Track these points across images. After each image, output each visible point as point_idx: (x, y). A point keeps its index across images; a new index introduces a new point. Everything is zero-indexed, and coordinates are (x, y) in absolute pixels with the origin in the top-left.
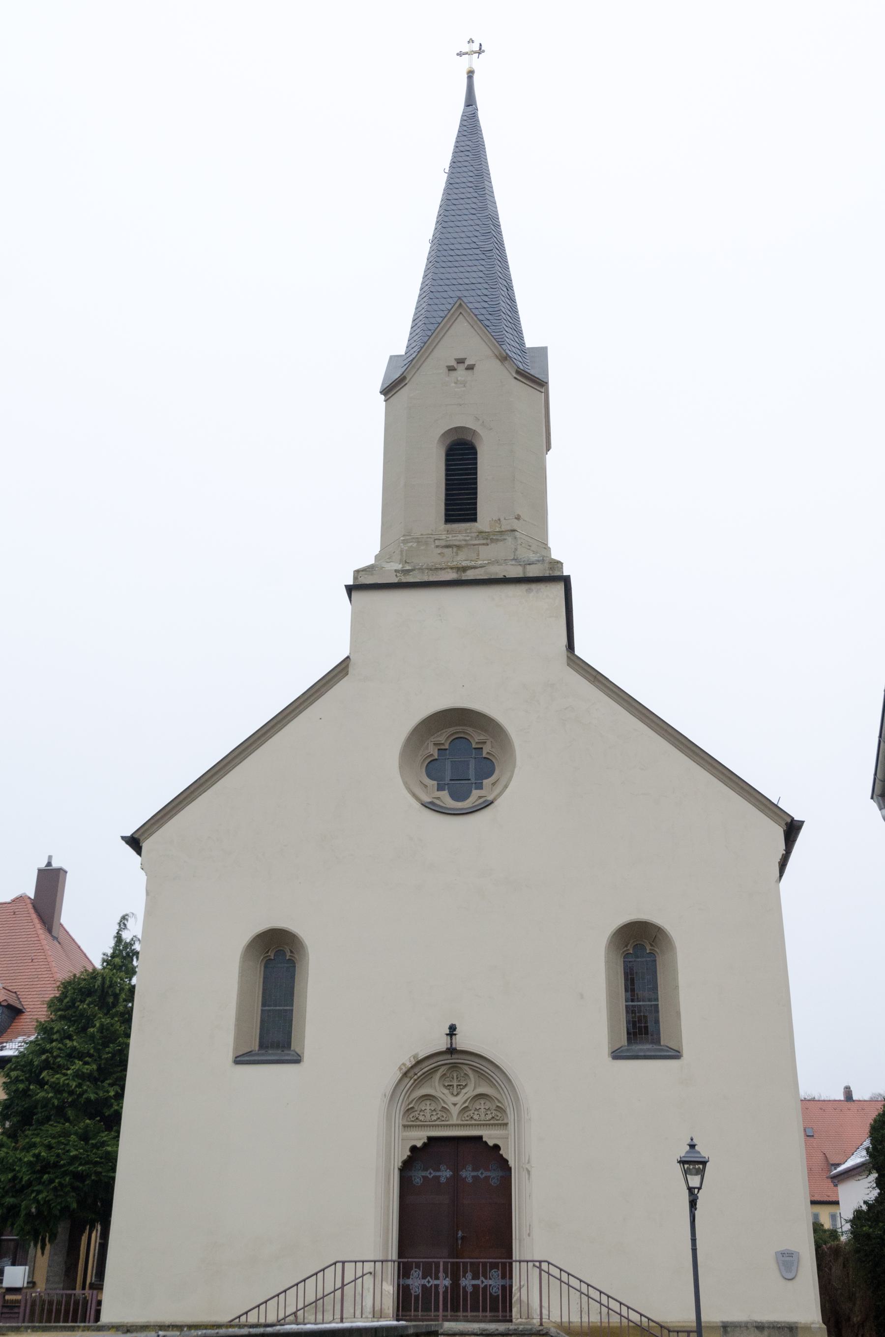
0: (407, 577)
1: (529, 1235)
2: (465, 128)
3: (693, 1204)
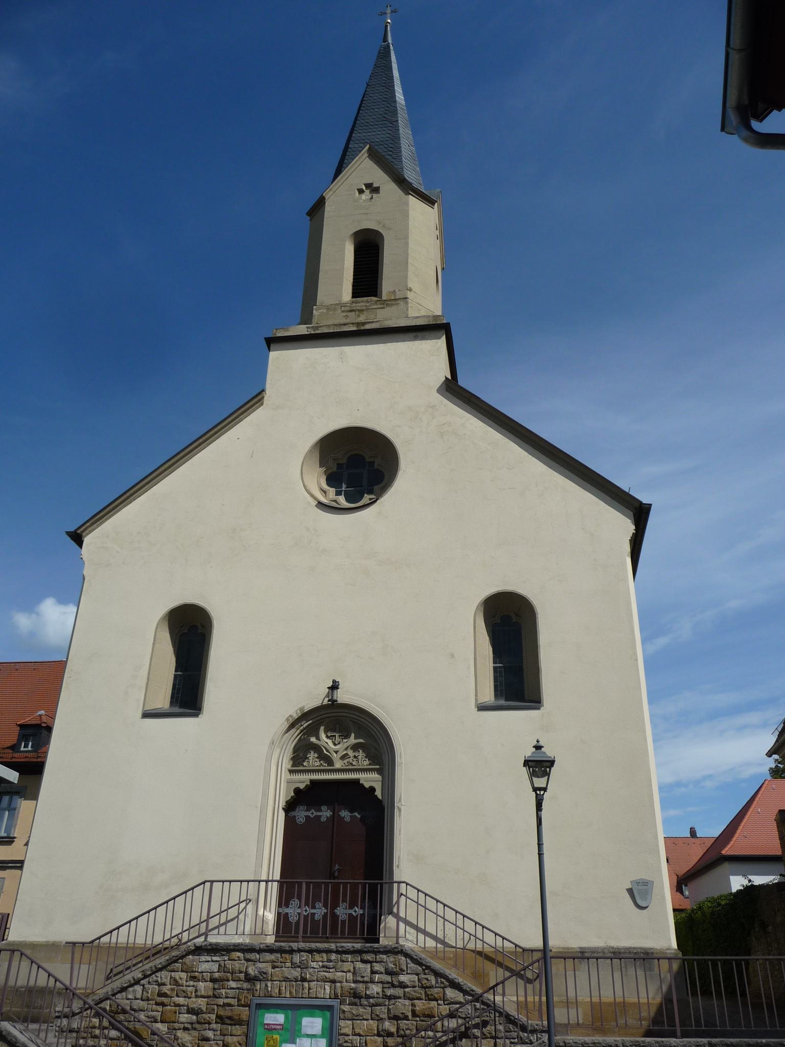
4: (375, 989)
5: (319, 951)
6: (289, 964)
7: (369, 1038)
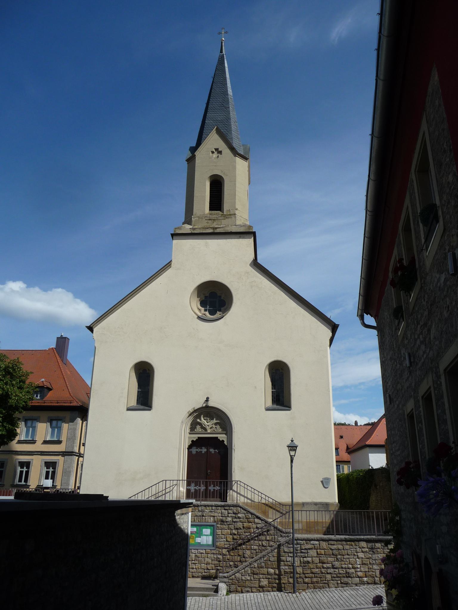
0: (194, 231)
1: (234, 472)
2: (220, 61)
3: (292, 461)
4: (229, 519)
5: (208, 506)
6: (197, 511)
7: (227, 536)
